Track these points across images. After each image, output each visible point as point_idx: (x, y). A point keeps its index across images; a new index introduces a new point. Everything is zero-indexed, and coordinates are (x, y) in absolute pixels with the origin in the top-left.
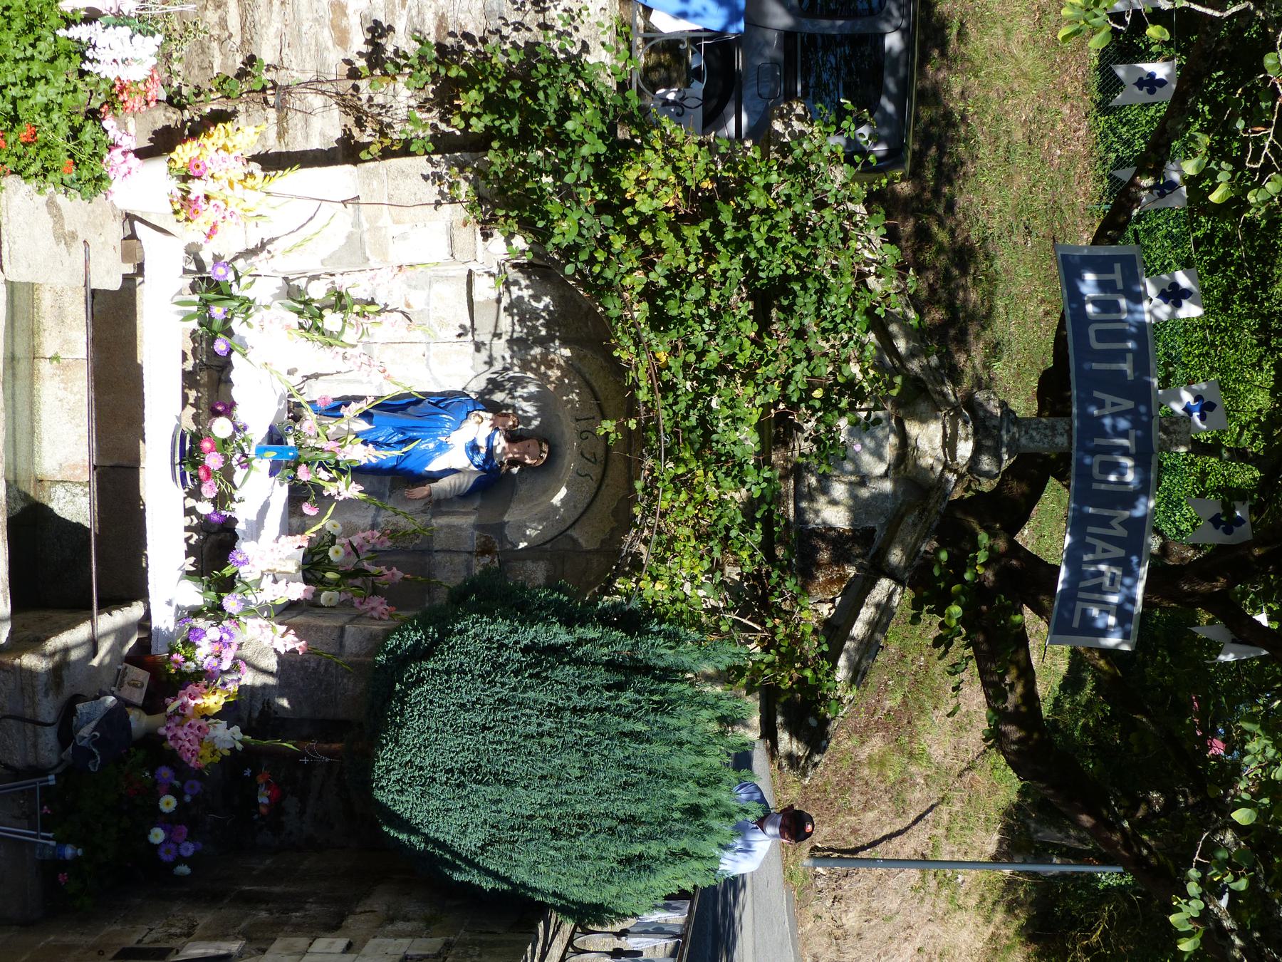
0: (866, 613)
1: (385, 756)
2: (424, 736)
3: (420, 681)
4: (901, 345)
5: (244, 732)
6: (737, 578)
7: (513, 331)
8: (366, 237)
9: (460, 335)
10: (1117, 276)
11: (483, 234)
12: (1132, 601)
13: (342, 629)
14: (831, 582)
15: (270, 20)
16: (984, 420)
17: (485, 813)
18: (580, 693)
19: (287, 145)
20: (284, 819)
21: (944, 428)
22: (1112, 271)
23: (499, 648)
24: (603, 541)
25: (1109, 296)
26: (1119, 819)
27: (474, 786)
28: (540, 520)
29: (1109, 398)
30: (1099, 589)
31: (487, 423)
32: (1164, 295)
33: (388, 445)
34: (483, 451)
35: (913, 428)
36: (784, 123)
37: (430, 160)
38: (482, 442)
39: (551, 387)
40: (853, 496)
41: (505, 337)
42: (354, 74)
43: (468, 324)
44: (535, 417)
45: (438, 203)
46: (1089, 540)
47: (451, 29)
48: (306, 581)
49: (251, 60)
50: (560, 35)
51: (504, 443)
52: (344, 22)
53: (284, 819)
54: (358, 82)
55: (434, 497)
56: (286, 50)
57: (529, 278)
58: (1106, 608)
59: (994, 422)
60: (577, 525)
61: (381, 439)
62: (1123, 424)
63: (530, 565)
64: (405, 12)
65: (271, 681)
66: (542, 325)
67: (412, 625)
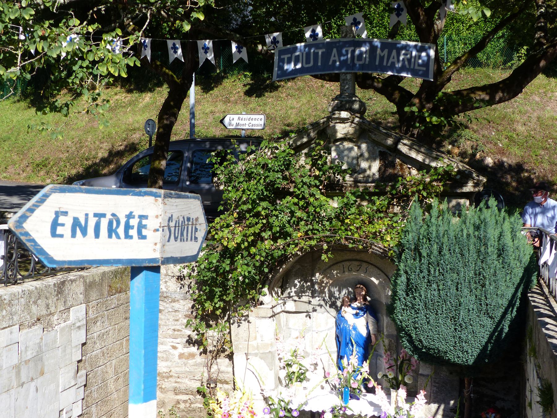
1: (451, 357)
2: (441, 340)
3: (420, 341)
4: (305, 140)
6: (399, 207)
7: (308, 296)
8: (261, 351)
9: (310, 318)
10: (286, 57)
12: (416, 46)
15: (184, 383)
17: (474, 316)
23: (407, 306)
26: (543, 49)
29: (332, 58)
30: (409, 60)
34: (358, 311)
35: (339, 135)
37: (233, 324)
38: (354, 312)
39: (331, 282)
40: (367, 160)
41: (311, 299)
42: (205, 352)
43: (306, 314)
44: (348, 290)
45: (249, 322)
46: (389, 64)
47: (190, 313)
48: (398, 388)
49: (199, 392)
50: (193, 271)
51: (357, 303)
52: (186, 354)
54: (208, 350)
55: (376, 333)
56: (196, 378)
57: (287, 288)
64: (183, 330)
65: (442, 407)
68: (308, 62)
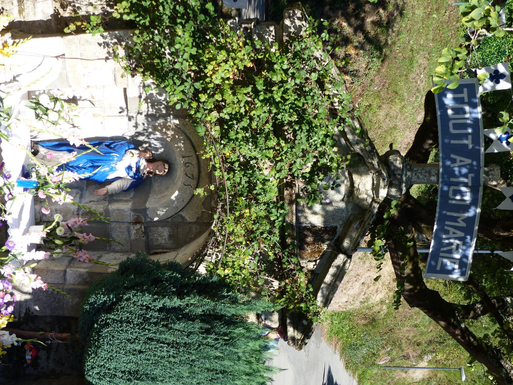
0: (332, 270)
3: (107, 325)
5: (17, 336)
7: (148, 111)
9: (120, 112)
10: (465, 95)
11: (132, 75)
12: (466, 257)
13: (65, 272)
14: (314, 252)
16: (393, 171)
18: (188, 336)
19: (24, 18)
20: (39, 361)
21: (373, 180)
22: (462, 92)
24: (198, 218)
25: (460, 106)
27: (136, 381)
28: (165, 207)
29: (458, 158)
31: (136, 156)
32: (492, 78)
33: (85, 168)
34: (134, 170)
36: (291, 21)
41: (144, 114)
43: (124, 106)
44: (160, 148)
45: (107, 59)
46: (446, 228)
53: (39, 361)
55: (110, 193)
58: (453, 260)
59: (400, 172)
60: (184, 210)
61: (80, 165)
62: (464, 171)
63: (160, 229)
66: (163, 108)
67: (102, 291)
68: (456, 126)
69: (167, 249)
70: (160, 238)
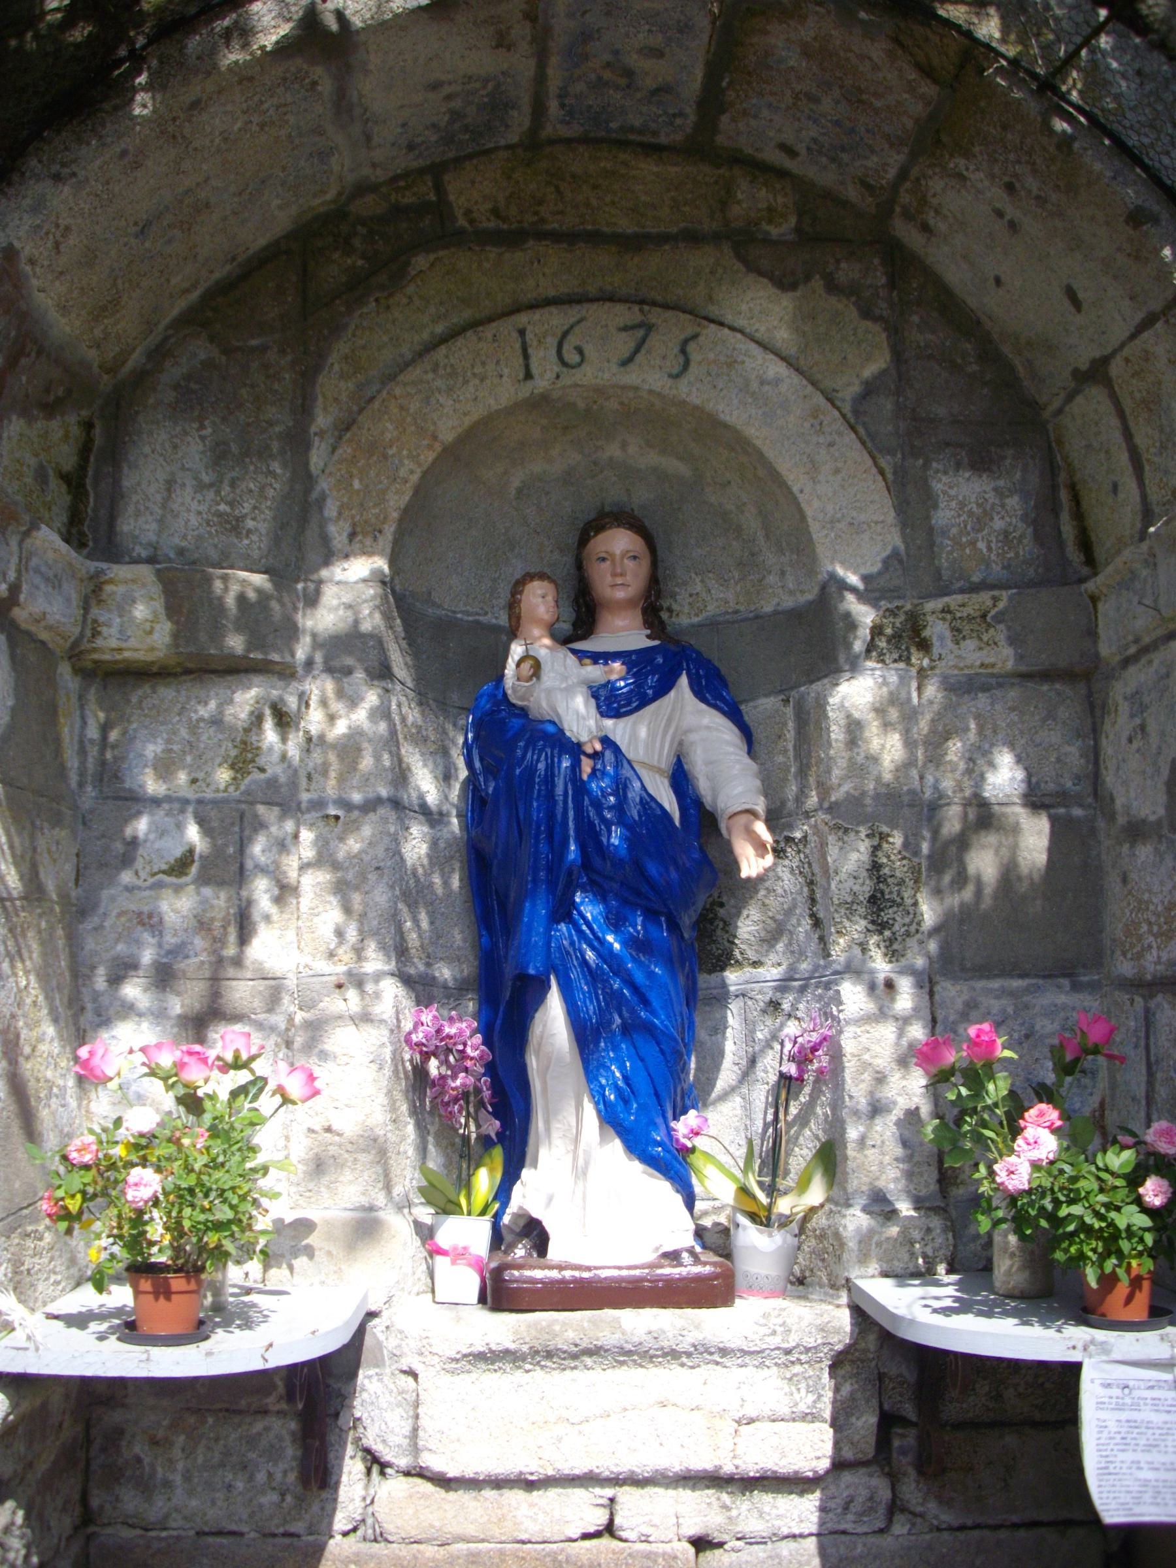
69: (1054, 488)
70: (998, 524)
